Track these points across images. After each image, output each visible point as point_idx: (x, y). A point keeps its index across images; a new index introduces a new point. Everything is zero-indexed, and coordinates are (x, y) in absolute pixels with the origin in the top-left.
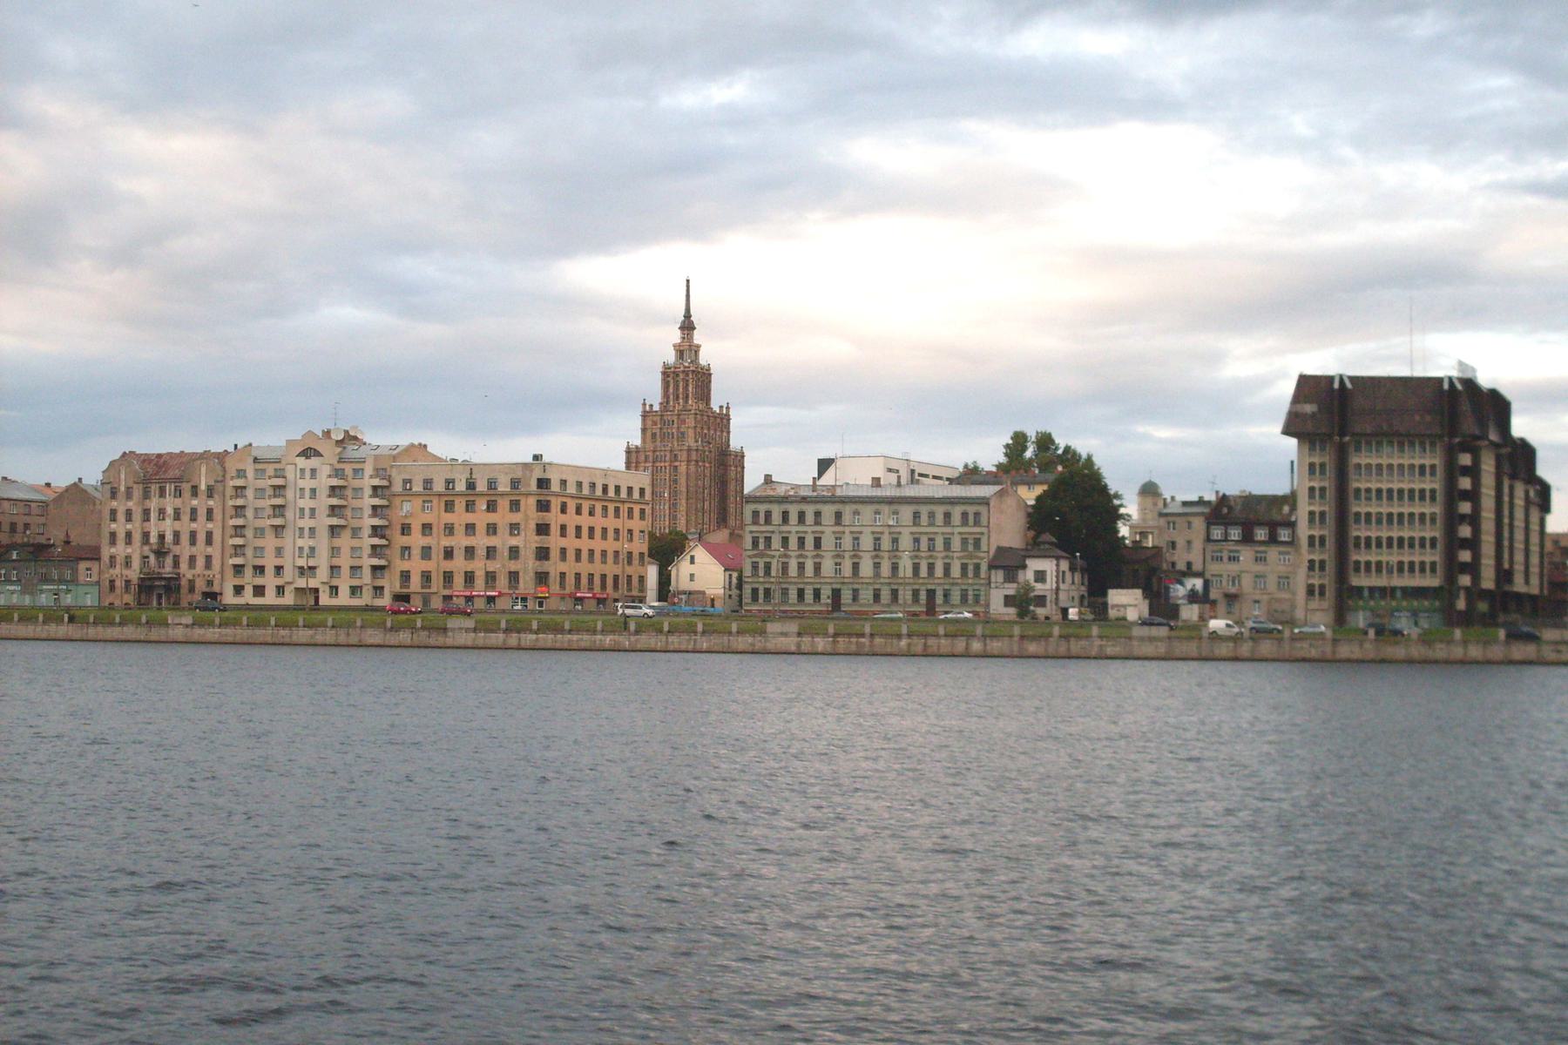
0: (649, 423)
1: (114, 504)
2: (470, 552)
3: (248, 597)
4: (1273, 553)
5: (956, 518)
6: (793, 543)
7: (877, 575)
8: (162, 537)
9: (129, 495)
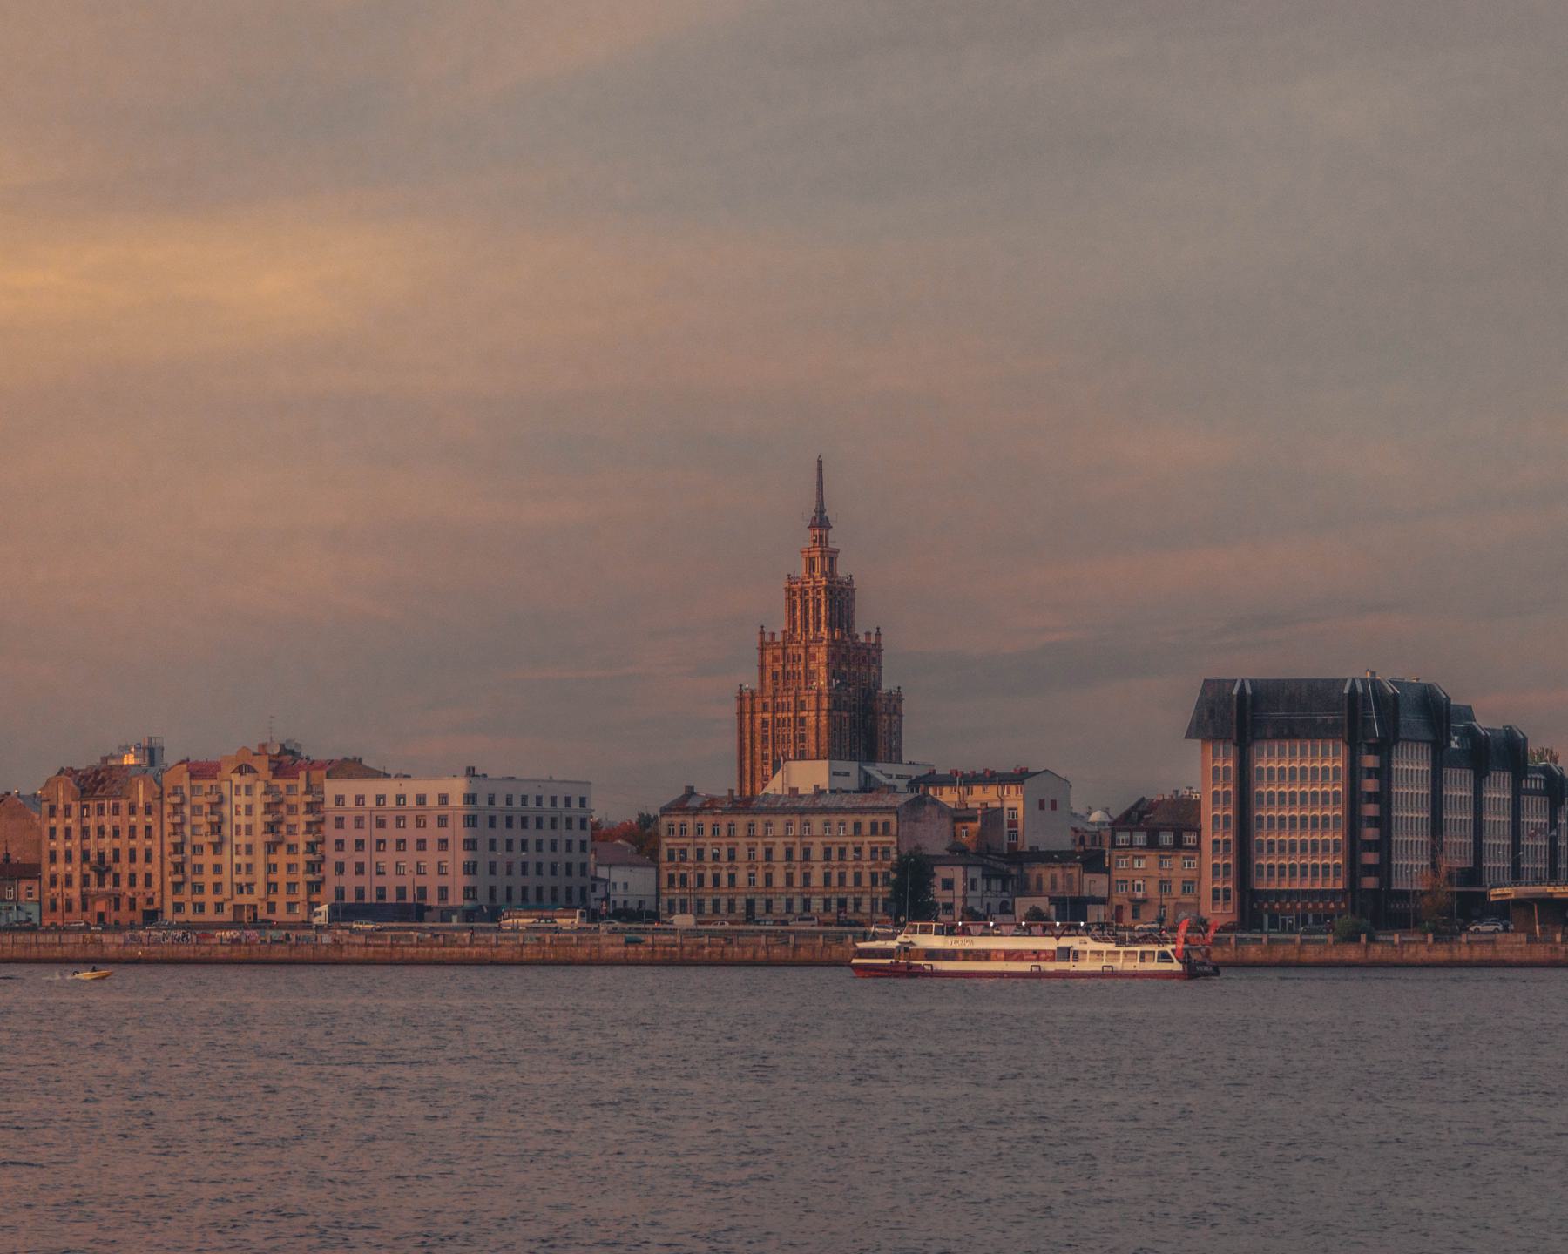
0: (769, 659)
1: (53, 821)
3: (188, 915)
8: (101, 855)
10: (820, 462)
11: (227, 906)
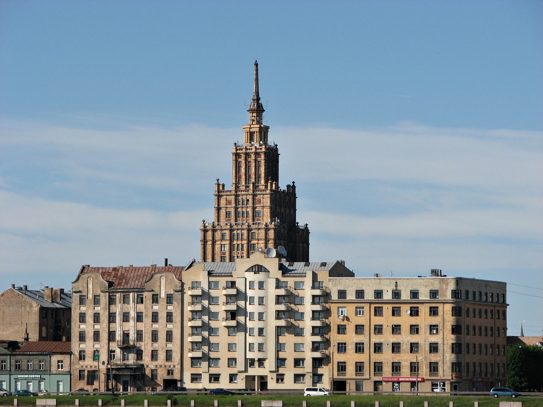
3: (205, 384)
8: (126, 335)
10: (257, 65)
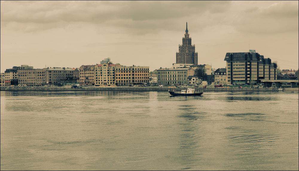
1: (81, 72)
2: (125, 78)
4: (224, 76)
5: (183, 72)
6: (163, 76)
7: (173, 80)
8: (87, 76)
9: (83, 71)
11: (103, 83)
